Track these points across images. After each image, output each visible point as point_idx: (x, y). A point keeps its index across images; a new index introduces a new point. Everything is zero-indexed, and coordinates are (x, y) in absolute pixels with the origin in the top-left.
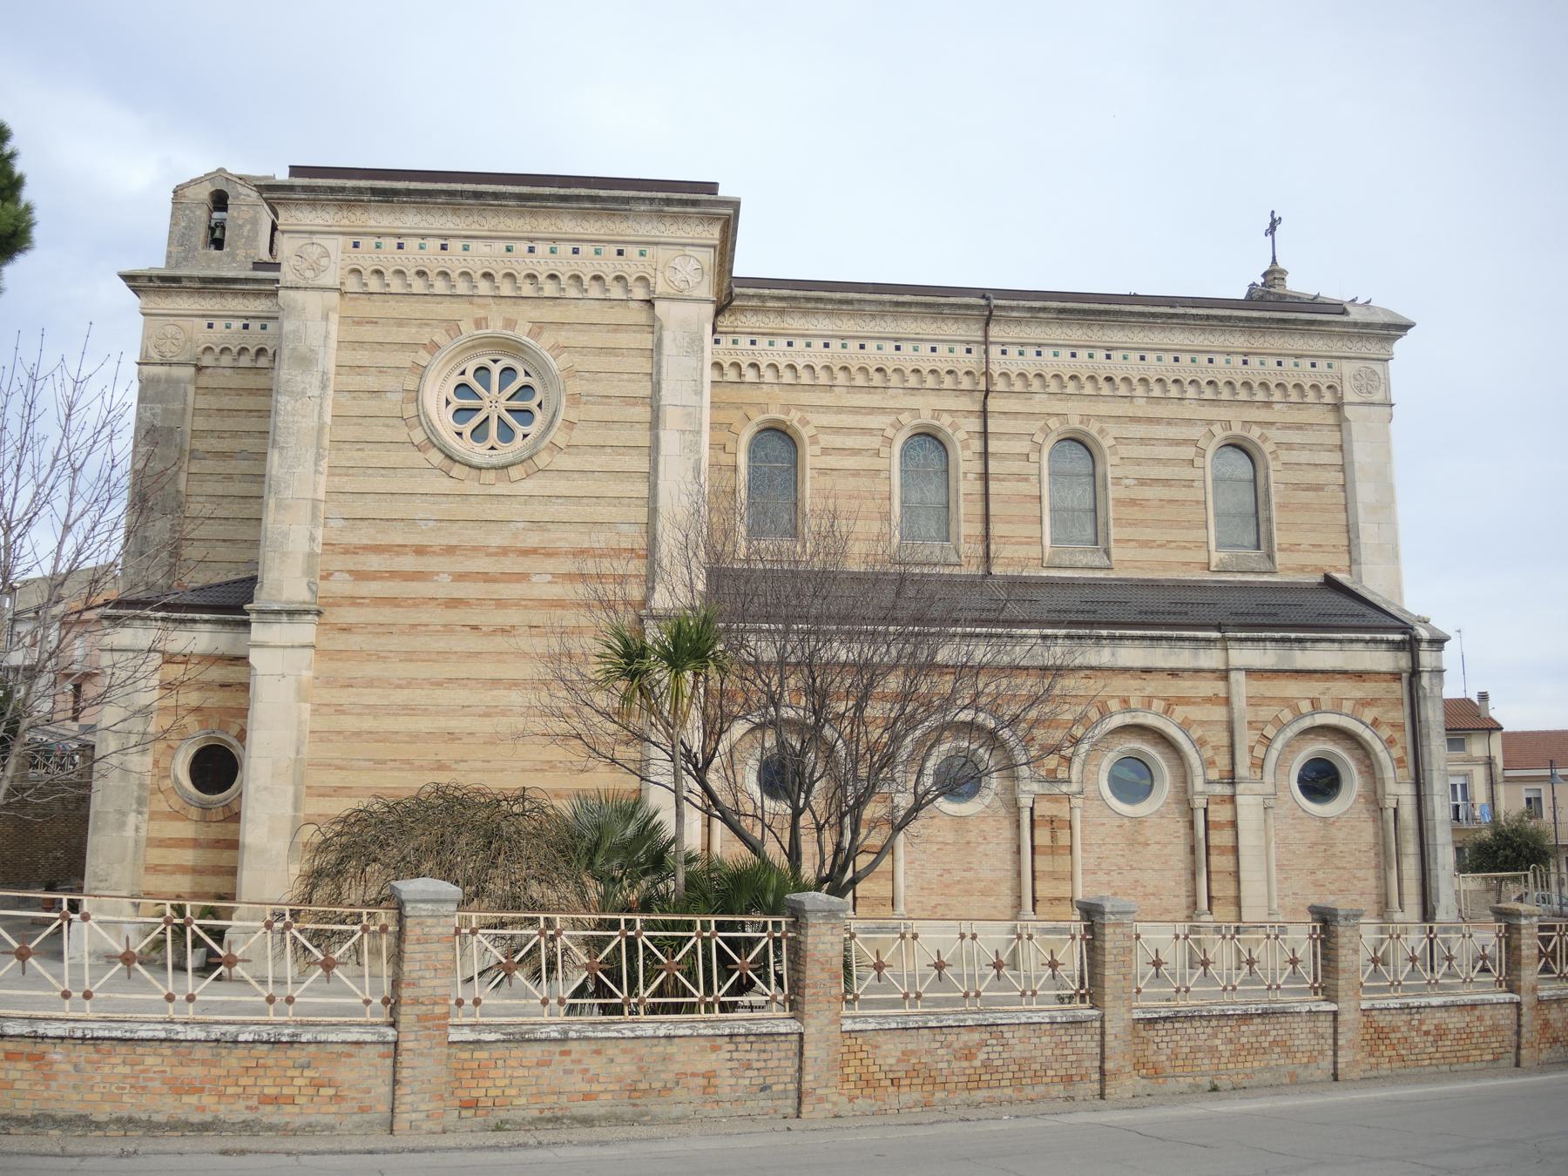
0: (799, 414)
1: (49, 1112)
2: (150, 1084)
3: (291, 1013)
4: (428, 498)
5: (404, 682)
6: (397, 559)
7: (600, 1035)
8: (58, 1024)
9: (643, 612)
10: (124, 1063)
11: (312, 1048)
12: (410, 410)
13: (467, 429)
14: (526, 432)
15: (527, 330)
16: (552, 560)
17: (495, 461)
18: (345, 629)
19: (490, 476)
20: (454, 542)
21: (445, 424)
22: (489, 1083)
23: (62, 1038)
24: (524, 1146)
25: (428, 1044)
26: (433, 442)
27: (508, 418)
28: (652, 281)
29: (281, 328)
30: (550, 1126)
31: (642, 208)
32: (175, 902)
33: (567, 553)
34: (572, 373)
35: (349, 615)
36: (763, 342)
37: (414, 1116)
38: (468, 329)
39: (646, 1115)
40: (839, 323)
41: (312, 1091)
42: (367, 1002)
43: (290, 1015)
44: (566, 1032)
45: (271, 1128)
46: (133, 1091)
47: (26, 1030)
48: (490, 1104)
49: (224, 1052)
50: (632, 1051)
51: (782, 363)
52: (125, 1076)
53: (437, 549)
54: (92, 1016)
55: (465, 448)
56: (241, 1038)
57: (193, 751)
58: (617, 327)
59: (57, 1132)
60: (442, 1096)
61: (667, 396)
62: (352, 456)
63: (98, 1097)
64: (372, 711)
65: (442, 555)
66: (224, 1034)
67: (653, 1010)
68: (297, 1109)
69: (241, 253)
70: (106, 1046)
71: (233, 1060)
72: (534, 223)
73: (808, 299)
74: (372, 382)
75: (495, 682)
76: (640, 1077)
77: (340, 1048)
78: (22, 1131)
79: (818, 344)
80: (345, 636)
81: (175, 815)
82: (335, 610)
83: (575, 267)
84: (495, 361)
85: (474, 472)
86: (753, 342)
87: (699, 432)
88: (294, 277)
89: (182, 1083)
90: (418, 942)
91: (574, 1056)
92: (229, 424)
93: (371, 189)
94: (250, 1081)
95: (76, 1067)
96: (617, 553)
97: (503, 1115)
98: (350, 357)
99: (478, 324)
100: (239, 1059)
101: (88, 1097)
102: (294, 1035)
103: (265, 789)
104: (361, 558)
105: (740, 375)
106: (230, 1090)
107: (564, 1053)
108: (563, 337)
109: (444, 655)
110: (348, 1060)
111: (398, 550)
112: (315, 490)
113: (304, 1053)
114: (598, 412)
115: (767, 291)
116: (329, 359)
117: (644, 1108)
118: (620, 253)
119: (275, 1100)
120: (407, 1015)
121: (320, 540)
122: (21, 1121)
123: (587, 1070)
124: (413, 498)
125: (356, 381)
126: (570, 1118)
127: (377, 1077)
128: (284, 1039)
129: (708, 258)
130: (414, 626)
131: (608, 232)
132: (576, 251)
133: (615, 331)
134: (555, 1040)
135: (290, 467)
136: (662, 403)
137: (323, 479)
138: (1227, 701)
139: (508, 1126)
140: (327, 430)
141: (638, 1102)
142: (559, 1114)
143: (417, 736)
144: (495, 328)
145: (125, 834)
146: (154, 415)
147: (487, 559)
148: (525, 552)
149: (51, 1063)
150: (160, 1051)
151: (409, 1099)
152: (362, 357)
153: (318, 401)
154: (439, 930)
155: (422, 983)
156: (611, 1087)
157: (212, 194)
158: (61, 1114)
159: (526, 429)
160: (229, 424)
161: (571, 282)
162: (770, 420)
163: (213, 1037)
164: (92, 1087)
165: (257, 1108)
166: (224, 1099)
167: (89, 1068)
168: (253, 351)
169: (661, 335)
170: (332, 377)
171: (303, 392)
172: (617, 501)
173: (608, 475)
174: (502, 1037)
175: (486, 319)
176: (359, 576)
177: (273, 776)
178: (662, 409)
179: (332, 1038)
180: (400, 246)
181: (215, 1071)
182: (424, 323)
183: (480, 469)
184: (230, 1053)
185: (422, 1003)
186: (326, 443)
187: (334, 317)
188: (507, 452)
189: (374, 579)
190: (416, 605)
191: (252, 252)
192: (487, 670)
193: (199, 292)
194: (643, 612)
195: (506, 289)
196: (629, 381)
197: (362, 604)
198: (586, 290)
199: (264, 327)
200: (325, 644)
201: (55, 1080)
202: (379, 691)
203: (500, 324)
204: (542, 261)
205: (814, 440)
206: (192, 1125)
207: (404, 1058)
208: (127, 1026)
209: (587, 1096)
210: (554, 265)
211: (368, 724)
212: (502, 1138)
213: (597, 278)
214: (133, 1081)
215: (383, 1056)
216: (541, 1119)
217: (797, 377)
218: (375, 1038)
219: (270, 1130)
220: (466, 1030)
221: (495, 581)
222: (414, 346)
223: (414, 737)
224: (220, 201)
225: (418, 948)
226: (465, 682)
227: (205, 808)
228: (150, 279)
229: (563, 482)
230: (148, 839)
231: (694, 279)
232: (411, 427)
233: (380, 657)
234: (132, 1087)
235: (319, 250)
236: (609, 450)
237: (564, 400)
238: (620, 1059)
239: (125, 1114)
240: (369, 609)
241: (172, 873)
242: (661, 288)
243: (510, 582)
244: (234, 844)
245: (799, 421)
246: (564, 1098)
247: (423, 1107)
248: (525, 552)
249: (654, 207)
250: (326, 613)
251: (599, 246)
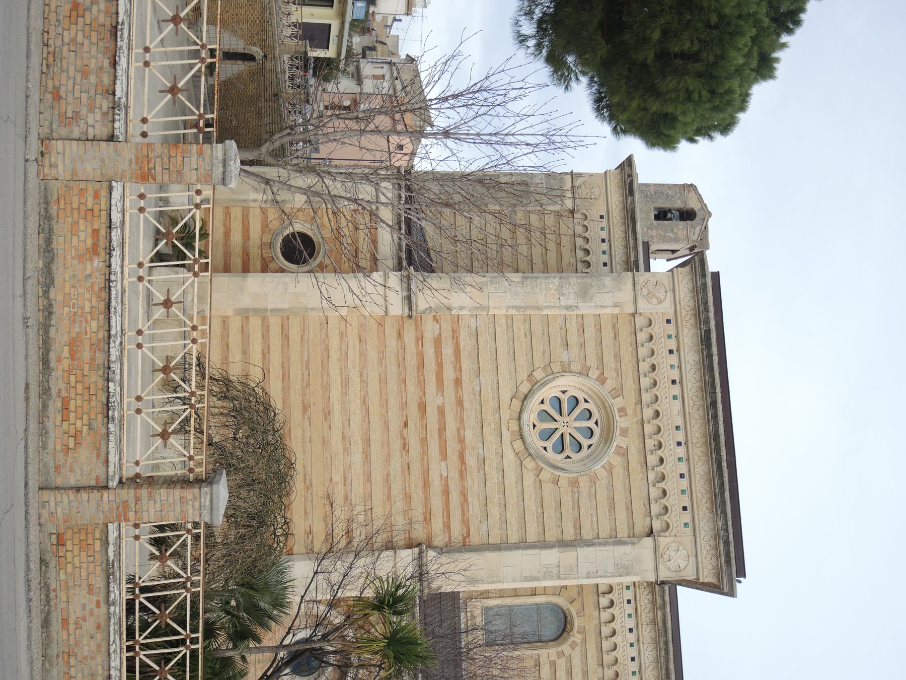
0: (578, 641)
1: (56, 259)
2: (77, 325)
3: (129, 412)
4: (496, 385)
5: (365, 378)
6: (451, 366)
7: (112, 628)
8: (119, 262)
9: (424, 547)
10: (92, 307)
11: (104, 431)
12: (556, 368)
13: (546, 407)
14: (548, 449)
15: (621, 445)
16: (457, 476)
17: (526, 429)
18: (400, 335)
19: (514, 426)
20: (465, 405)
21: (549, 391)
22: (76, 552)
23: (110, 266)
24: (29, 588)
25: (106, 509)
26: (535, 385)
27: (557, 436)
28: (667, 534)
29: (606, 275)
30: (43, 597)
31: (719, 523)
33: (463, 487)
34: (594, 480)
35: (410, 336)
36: (630, 609)
37: (52, 504)
38: (617, 403)
39: (50, 665)
40: (651, 668)
41: (72, 432)
42: (137, 463)
43: (128, 412)
44: (114, 604)
45: (45, 406)
46: (72, 314)
47: (115, 243)
48: (61, 554)
49: (101, 373)
50: (99, 651)
51: (616, 625)
52: (83, 308)
53: (460, 393)
54: (126, 283)
55: (534, 405)
56: (111, 384)
57: (310, 233)
58: (630, 510)
59: (41, 265)
60: (68, 521)
61: (584, 552)
62: (520, 329)
63: (67, 291)
64: (344, 358)
65: (456, 397)
66: (114, 372)
67: (131, 661)
68: (58, 423)
69: (654, 233)
70: (104, 295)
71: (95, 379)
72: (699, 445)
73: (666, 643)
74: (574, 339)
75: (367, 442)
76: (79, 659)
77: (103, 449)
78: (42, 242)
79: (633, 652)
80: (395, 335)
81: (265, 226)
82: (413, 327)
83: (671, 477)
84: (596, 423)
85: (516, 415)
86: (629, 602)
87: (559, 578)
88: (641, 281)
89: (79, 346)
90: (181, 498)
91: (96, 611)
93: (709, 330)
94: (79, 390)
95: (90, 276)
96: (466, 522)
97: (52, 564)
98: (590, 323)
99: (622, 410)
100: (96, 383)
101: (67, 285)
102: (113, 419)
103: (286, 289)
104: (450, 341)
105: (604, 593)
106: (73, 378)
107: (98, 603)
108: (619, 471)
109: (385, 404)
110: (94, 455)
111: (458, 367)
112: (495, 308)
113: (100, 426)
114: (567, 501)
115: (668, 610)
116: (587, 309)
117: (55, 662)
118: (685, 508)
119: (65, 408)
120: (128, 494)
121: (461, 313)
122: (48, 242)
123: (85, 620)
124: (495, 374)
125: (573, 329)
126: (49, 611)
127: (82, 475)
128: (110, 413)
129: (690, 575)
130: (405, 381)
131: (699, 499)
132: (682, 476)
133: (627, 509)
134: (108, 597)
135: (510, 290)
136: (578, 549)
137: (503, 312)
139: (43, 568)
140: (537, 312)
141: (60, 659)
142: (52, 603)
143: (327, 390)
144: (621, 422)
145: (251, 192)
147: (455, 429)
148: (462, 457)
149: (91, 260)
150: (101, 330)
151: (65, 500)
152: (590, 332)
153: (558, 305)
154: (190, 511)
155: (152, 503)
156: (72, 638)
157: (693, 210)
158: (54, 267)
159: (550, 449)
161: (660, 474)
162: (572, 618)
163: (112, 365)
164: (74, 287)
165: (60, 396)
166: (66, 374)
167: (88, 284)
168: (587, 247)
169: (628, 544)
170: (575, 312)
171: (562, 294)
172: (503, 519)
173: (522, 512)
174: (111, 560)
175: (626, 415)
176: (438, 341)
177: (295, 293)
178: (574, 549)
179: (111, 445)
180: (671, 352)
181: (86, 367)
182: (619, 372)
183: (519, 419)
184: (100, 376)
185: (136, 503)
186: (529, 312)
187: (616, 311)
188: (533, 437)
189: (436, 352)
190: (419, 382)
191: (655, 240)
192: (376, 436)
193: (625, 208)
194: (424, 547)
195: (649, 429)
196: (592, 522)
197: (418, 345)
198: (654, 486)
199: (604, 253)
200: (388, 322)
201: (79, 262)
202: (358, 361)
203: (624, 425)
204: (671, 452)
205: (561, 654)
206: (47, 354)
207: (96, 495)
208: (119, 308)
209: (65, 622)
210: (670, 461)
211: (334, 355)
212: (34, 566)
213: (664, 493)
214: (79, 314)
215: (97, 478)
216: (48, 590)
217: (607, 637)
218: (111, 473)
219: (43, 406)
220: (116, 534)
221: (440, 436)
222: (601, 366)
223: (326, 388)
224: (687, 215)
225: (177, 498)
226: (367, 420)
227: (271, 245)
228: (630, 176)
229: (514, 479)
230: (248, 208)
231: (672, 565)
232: (544, 369)
233: (382, 360)
234: (75, 313)
235: (662, 297)
236: (540, 511)
237: (574, 475)
238: (93, 643)
239: (54, 310)
240: (414, 350)
241: (225, 225)
242: (663, 541)
243: (440, 446)
244: (246, 269)
245: (574, 642)
246: (64, 605)
247: (59, 510)
248: (462, 457)
249: (721, 532)
250: (410, 321)
251: (688, 492)
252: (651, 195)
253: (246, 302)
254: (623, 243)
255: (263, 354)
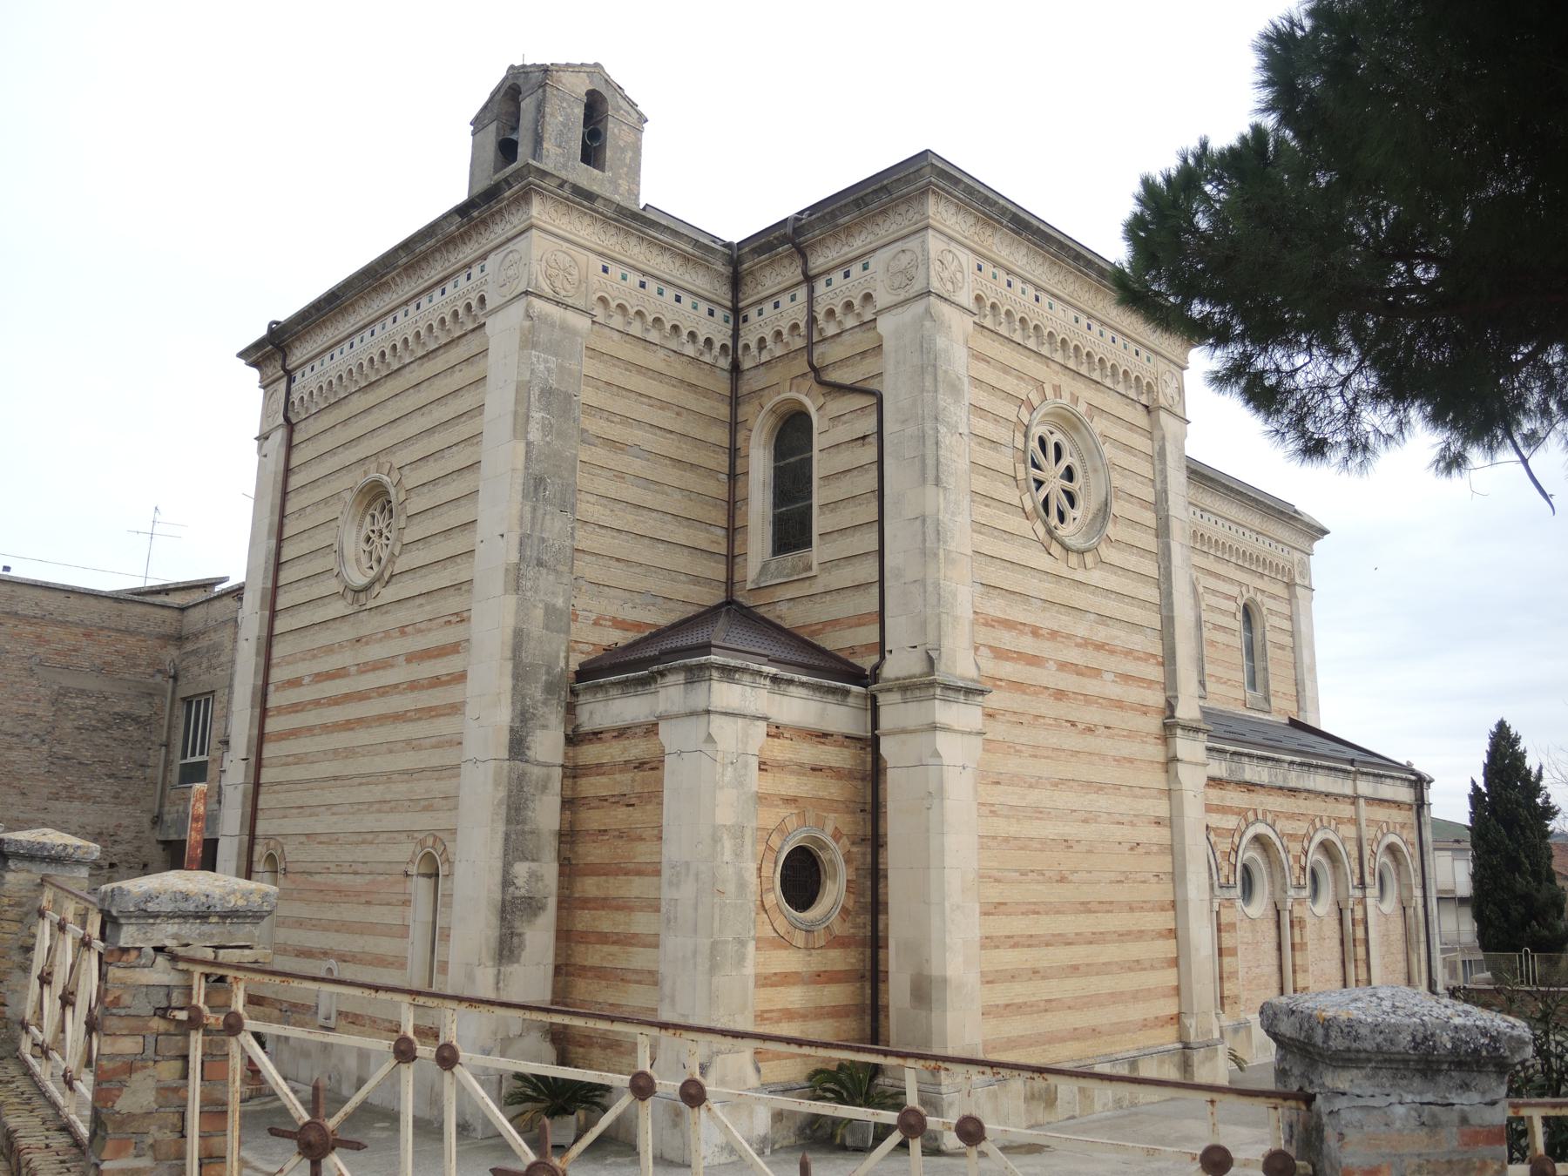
32: (1552, 1113)
33: (1122, 652)
92: (620, 405)
138: (574, 739)
146: (548, 370)
160: (620, 405)
193: (606, 220)
226: (1071, 783)
252: (563, 155)
253: (973, 978)
254: (655, 251)
255: (1015, 946)
